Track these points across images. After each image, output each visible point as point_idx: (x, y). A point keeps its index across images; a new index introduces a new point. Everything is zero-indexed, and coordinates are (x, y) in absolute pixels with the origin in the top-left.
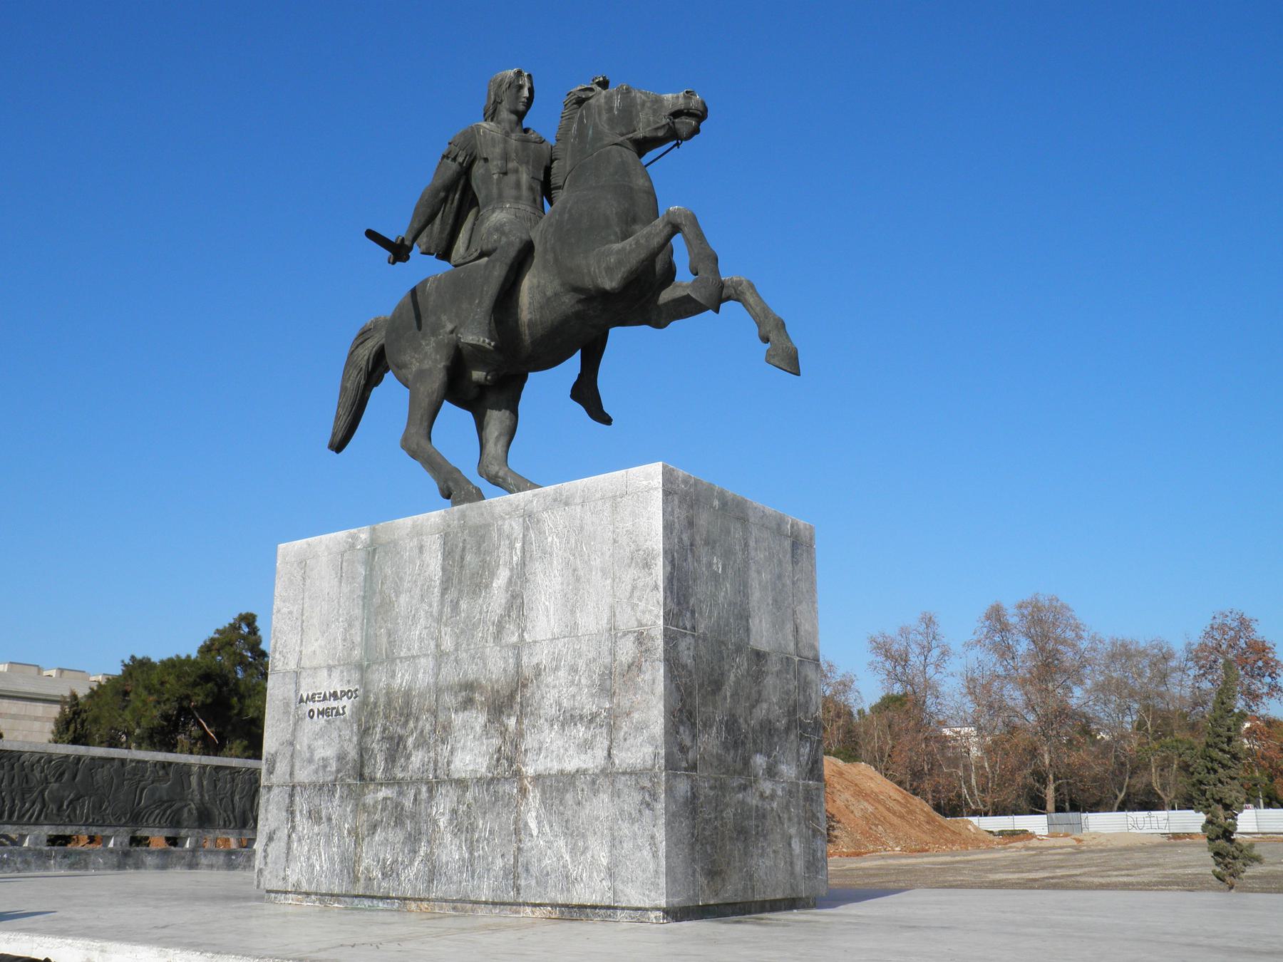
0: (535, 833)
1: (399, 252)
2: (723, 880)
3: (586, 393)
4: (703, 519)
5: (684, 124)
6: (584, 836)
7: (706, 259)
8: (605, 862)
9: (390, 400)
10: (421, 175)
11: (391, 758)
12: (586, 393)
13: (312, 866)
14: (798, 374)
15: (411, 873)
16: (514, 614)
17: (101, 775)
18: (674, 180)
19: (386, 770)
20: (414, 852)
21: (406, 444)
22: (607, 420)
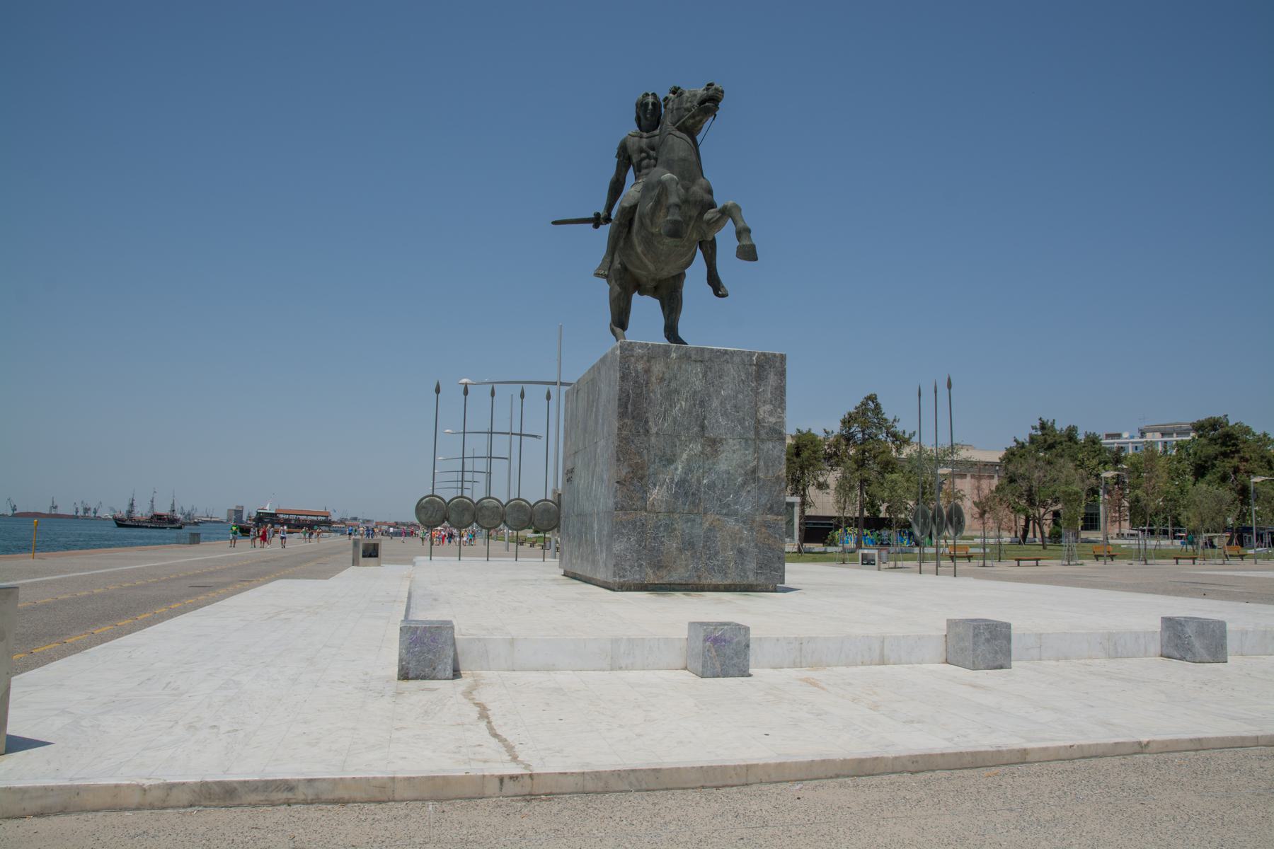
12: (714, 281)
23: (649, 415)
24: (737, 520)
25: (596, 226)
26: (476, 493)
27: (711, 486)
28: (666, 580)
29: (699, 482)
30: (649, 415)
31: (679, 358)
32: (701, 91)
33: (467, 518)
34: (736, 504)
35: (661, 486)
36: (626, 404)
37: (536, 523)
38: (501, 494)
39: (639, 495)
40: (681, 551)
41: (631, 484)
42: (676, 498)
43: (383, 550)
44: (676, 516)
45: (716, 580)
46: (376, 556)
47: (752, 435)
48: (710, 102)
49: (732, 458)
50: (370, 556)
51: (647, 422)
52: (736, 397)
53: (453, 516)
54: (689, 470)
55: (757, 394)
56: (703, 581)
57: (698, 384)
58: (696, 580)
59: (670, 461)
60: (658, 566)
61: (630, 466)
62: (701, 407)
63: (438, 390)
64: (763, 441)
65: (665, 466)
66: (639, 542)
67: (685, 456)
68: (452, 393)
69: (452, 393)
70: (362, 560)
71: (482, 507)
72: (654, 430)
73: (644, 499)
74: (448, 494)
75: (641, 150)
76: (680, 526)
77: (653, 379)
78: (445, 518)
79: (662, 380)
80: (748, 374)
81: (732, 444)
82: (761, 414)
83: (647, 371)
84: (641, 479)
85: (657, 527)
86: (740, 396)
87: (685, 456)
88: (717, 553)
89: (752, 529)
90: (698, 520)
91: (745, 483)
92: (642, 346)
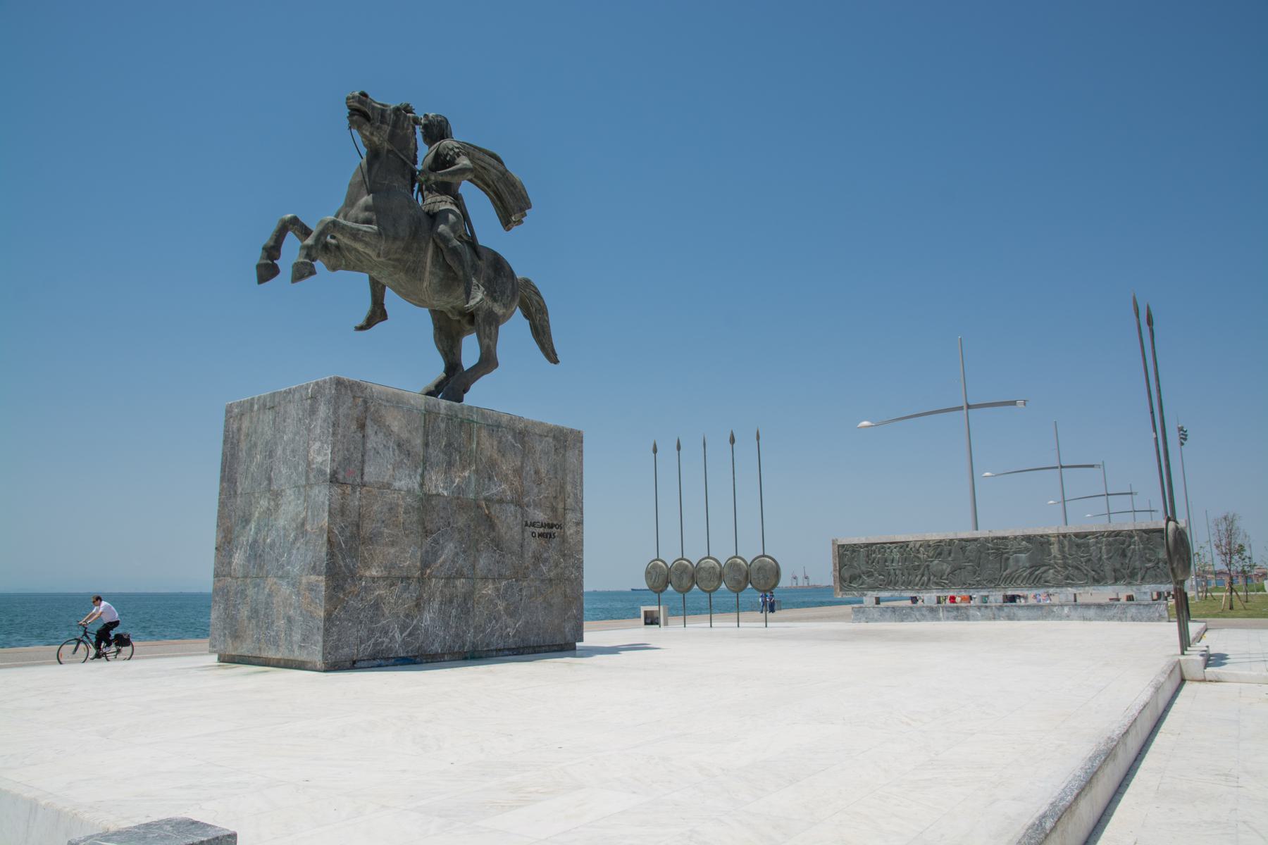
17: (971, 547)
26: (694, 555)
27: (272, 546)
29: (264, 541)
38: (723, 554)
40: (250, 618)
44: (249, 581)
50: (652, 623)
54: (258, 530)
55: (309, 430)
56: (264, 655)
58: (256, 653)
60: (236, 636)
63: (732, 440)
66: (225, 609)
67: (257, 514)
68: (667, 450)
69: (667, 450)
72: (239, 491)
73: (230, 564)
74: (670, 557)
77: (242, 438)
79: (248, 435)
80: (304, 410)
81: (290, 493)
82: (312, 454)
89: (298, 594)
91: (296, 539)
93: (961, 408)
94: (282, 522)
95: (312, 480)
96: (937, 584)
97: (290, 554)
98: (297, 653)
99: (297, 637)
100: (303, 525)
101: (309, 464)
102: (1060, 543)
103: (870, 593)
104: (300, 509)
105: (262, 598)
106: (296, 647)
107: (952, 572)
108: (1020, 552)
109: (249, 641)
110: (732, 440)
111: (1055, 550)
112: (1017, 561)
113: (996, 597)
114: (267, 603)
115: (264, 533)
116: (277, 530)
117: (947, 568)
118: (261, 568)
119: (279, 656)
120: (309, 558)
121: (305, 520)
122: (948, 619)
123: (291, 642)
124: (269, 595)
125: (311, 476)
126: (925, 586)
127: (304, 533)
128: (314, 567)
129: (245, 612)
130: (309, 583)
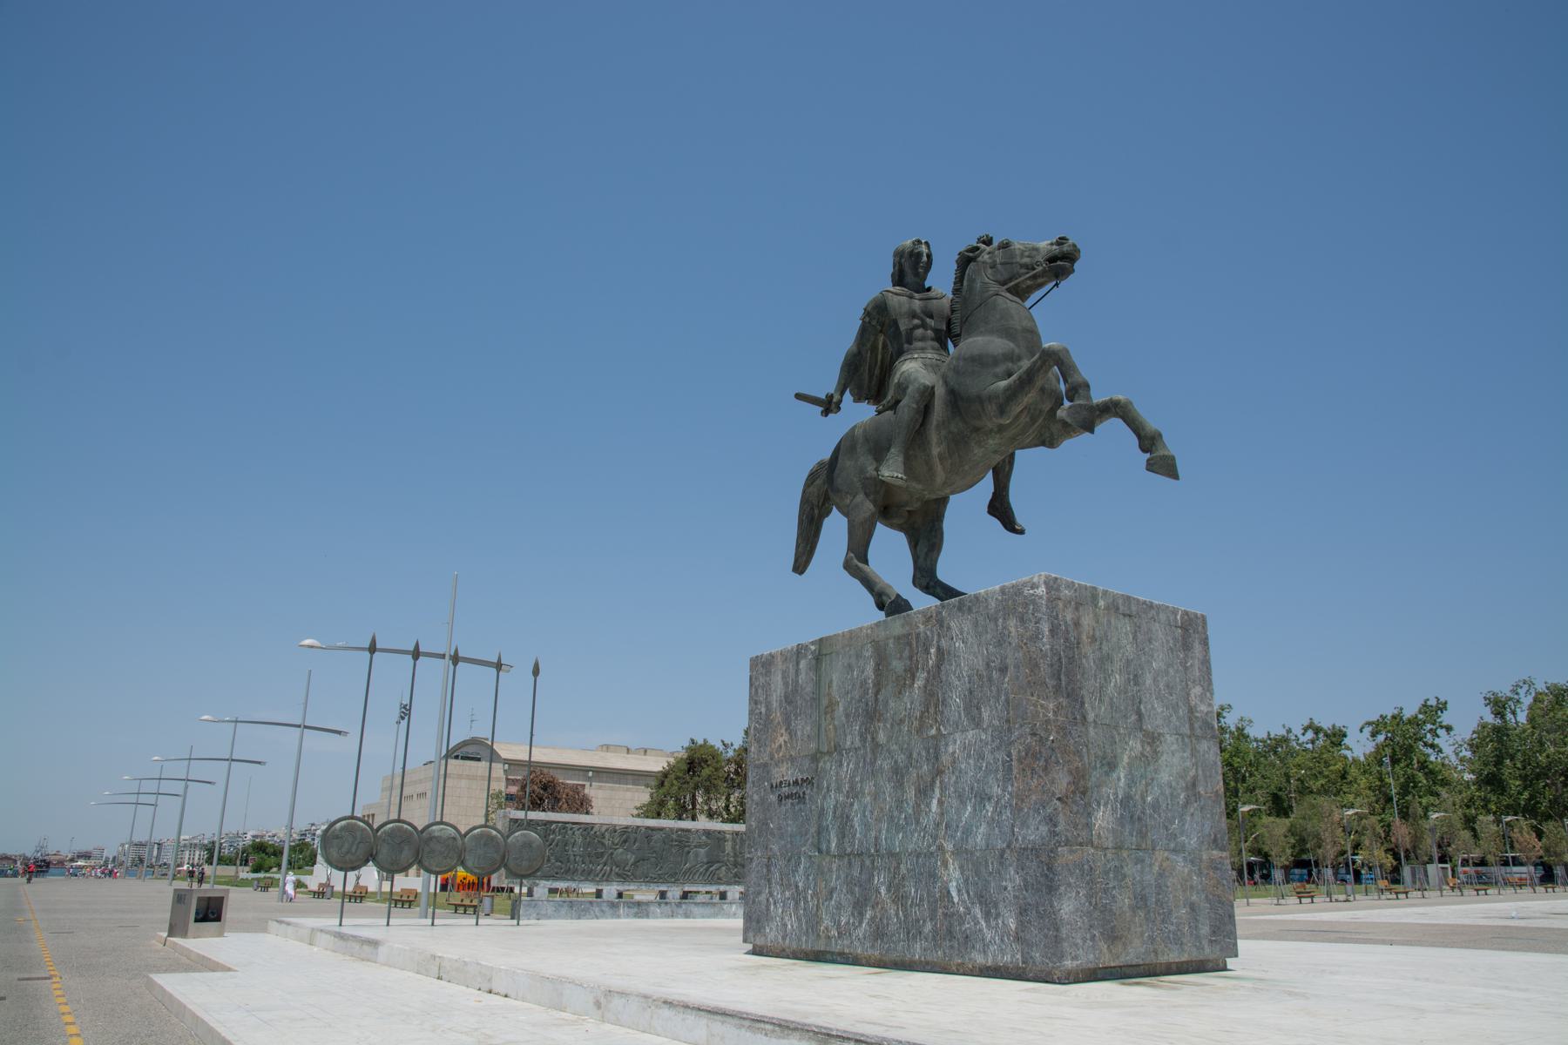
0: (956, 900)
1: (829, 406)
2: (1125, 944)
3: (1000, 509)
4: (1087, 621)
5: (1061, 263)
6: (996, 906)
7: (1078, 389)
8: (1013, 926)
9: (835, 528)
10: (844, 337)
11: (842, 836)
12: (1000, 509)
13: (785, 925)
14: (1175, 476)
15: (860, 932)
16: (932, 710)
17: (657, 836)
18: (1054, 317)
19: (838, 846)
20: (861, 914)
21: (847, 566)
22: (1021, 532)
23: (1084, 692)
24: (1185, 859)
25: (826, 412)
26: (418, 815)
27: (1156, 806)
28: (1124, 960)
29: (1143, 799)
30: (1084, 692)
31: (1107, 608)
32: (1044, 244)
33: (407, 854)
34: (1182, 833)
35: (1106, 805)
36: (1059, 672)
37: (511, 864)
39: (1084, 821)
40: (1134, 909)
41: (1074, 802)
42: (1123, 826)
43: (229, 913)
44: (1125, 854)
45: (1173, 956)
46: (218, 919)
47: (1186, 730)
48: (1061, 263)
49: (1173, 763)
51: (1083, 703)
52: (1167, 673)
53: (384, 852)
54: (1131, 782)
56: (1163, 959)
57: (1130, 650)
58: (1151, 959)
59: (1112, 766)
60: (1113, 937)
61: (1070, 772)
62: (1136, 684)
63: (536, 672)
64: (1198, 738)
65: (1107, 774)
66: (1089, 897)
67: (1126, 759)
70: (192, 925)
71: (431, 838)
72: (1091, 717)
73: (1089, 826)
75: (914, 315)
76: (1131, 870)
78: (371, 857)
83: (1077, 624)
84: (1084, 794)
85: (1107, 873)
86: (1171, 671)
87: (1126, 759)
88: (1170, 912)
89: (1200, 874)
90: (1148, 861)
91: (1187, 803)
92: (1070, 585)
93: (443, 656)
94: (1164, 777)
95: (1198, 732)
96: (618, 875)
97: (1182, 820)
98: (1207, 950)
99: (1205, 930)
100: (1194, 785)
101: (1191, 710)
102: (734, 841)
103: (543, 883)
104: (1188, 764)
105: (1150, 878)
106: (1205, 943)
107: (635, 864)
108: (700, 846)
109: (1137, 942)
110: (536, 672)
111: (728, 846)
112: (697, 855)
113: (674, 892)
114: (1159, 886)
115: (1142, 787)
116: (1160, 787)
117: (631, 858)
118: (1143, 835)
119: (1185, 958)
120: (1207, 829)
121: (1195, 778)
122: (628, 916)
123: (1198, 937)
124: (1161, 875)
125: (1196, 726)
126: (607, 879)
127: (1197, 796)
128: (1215, 840)
129: (1124, 901)
130: (1212, 861)
